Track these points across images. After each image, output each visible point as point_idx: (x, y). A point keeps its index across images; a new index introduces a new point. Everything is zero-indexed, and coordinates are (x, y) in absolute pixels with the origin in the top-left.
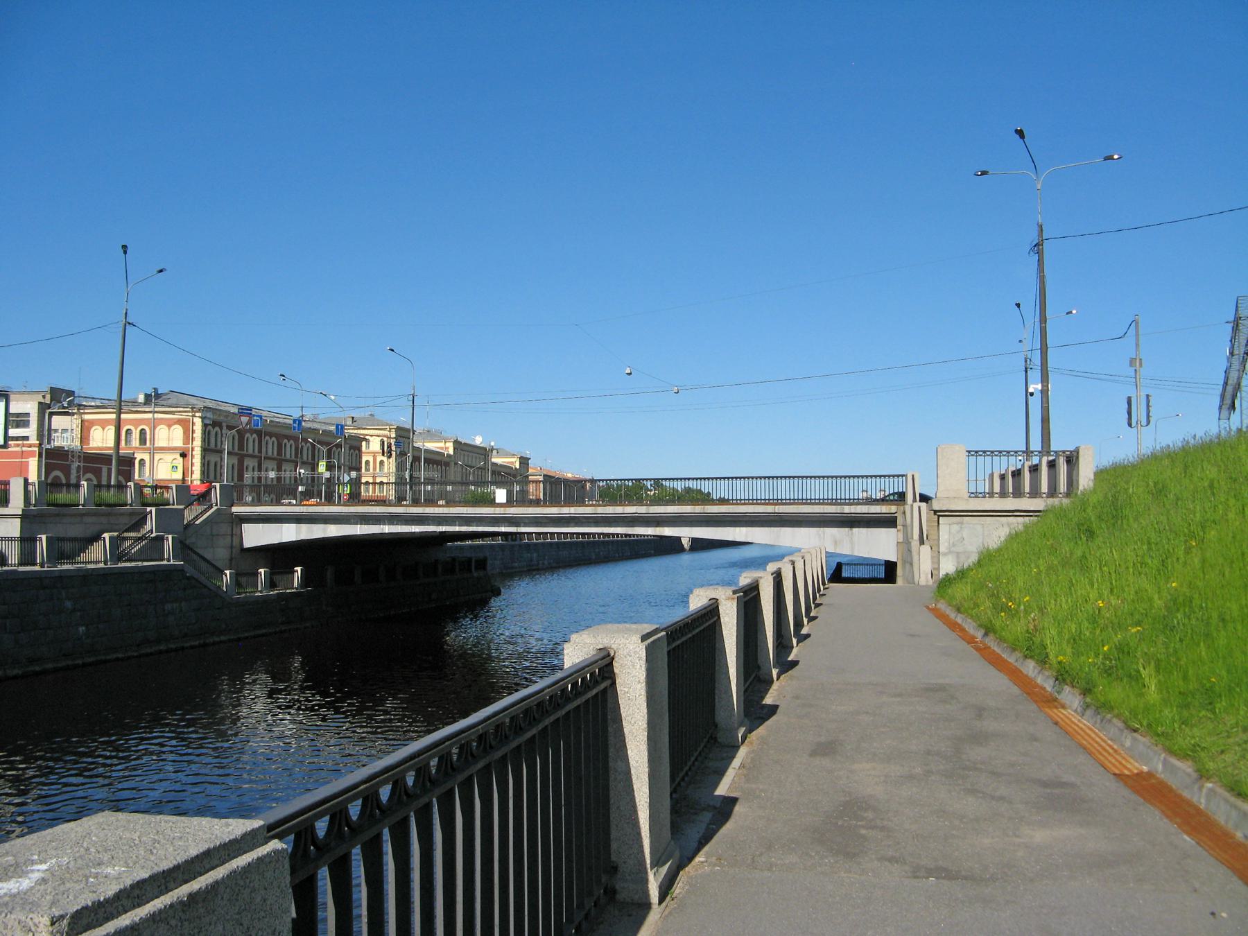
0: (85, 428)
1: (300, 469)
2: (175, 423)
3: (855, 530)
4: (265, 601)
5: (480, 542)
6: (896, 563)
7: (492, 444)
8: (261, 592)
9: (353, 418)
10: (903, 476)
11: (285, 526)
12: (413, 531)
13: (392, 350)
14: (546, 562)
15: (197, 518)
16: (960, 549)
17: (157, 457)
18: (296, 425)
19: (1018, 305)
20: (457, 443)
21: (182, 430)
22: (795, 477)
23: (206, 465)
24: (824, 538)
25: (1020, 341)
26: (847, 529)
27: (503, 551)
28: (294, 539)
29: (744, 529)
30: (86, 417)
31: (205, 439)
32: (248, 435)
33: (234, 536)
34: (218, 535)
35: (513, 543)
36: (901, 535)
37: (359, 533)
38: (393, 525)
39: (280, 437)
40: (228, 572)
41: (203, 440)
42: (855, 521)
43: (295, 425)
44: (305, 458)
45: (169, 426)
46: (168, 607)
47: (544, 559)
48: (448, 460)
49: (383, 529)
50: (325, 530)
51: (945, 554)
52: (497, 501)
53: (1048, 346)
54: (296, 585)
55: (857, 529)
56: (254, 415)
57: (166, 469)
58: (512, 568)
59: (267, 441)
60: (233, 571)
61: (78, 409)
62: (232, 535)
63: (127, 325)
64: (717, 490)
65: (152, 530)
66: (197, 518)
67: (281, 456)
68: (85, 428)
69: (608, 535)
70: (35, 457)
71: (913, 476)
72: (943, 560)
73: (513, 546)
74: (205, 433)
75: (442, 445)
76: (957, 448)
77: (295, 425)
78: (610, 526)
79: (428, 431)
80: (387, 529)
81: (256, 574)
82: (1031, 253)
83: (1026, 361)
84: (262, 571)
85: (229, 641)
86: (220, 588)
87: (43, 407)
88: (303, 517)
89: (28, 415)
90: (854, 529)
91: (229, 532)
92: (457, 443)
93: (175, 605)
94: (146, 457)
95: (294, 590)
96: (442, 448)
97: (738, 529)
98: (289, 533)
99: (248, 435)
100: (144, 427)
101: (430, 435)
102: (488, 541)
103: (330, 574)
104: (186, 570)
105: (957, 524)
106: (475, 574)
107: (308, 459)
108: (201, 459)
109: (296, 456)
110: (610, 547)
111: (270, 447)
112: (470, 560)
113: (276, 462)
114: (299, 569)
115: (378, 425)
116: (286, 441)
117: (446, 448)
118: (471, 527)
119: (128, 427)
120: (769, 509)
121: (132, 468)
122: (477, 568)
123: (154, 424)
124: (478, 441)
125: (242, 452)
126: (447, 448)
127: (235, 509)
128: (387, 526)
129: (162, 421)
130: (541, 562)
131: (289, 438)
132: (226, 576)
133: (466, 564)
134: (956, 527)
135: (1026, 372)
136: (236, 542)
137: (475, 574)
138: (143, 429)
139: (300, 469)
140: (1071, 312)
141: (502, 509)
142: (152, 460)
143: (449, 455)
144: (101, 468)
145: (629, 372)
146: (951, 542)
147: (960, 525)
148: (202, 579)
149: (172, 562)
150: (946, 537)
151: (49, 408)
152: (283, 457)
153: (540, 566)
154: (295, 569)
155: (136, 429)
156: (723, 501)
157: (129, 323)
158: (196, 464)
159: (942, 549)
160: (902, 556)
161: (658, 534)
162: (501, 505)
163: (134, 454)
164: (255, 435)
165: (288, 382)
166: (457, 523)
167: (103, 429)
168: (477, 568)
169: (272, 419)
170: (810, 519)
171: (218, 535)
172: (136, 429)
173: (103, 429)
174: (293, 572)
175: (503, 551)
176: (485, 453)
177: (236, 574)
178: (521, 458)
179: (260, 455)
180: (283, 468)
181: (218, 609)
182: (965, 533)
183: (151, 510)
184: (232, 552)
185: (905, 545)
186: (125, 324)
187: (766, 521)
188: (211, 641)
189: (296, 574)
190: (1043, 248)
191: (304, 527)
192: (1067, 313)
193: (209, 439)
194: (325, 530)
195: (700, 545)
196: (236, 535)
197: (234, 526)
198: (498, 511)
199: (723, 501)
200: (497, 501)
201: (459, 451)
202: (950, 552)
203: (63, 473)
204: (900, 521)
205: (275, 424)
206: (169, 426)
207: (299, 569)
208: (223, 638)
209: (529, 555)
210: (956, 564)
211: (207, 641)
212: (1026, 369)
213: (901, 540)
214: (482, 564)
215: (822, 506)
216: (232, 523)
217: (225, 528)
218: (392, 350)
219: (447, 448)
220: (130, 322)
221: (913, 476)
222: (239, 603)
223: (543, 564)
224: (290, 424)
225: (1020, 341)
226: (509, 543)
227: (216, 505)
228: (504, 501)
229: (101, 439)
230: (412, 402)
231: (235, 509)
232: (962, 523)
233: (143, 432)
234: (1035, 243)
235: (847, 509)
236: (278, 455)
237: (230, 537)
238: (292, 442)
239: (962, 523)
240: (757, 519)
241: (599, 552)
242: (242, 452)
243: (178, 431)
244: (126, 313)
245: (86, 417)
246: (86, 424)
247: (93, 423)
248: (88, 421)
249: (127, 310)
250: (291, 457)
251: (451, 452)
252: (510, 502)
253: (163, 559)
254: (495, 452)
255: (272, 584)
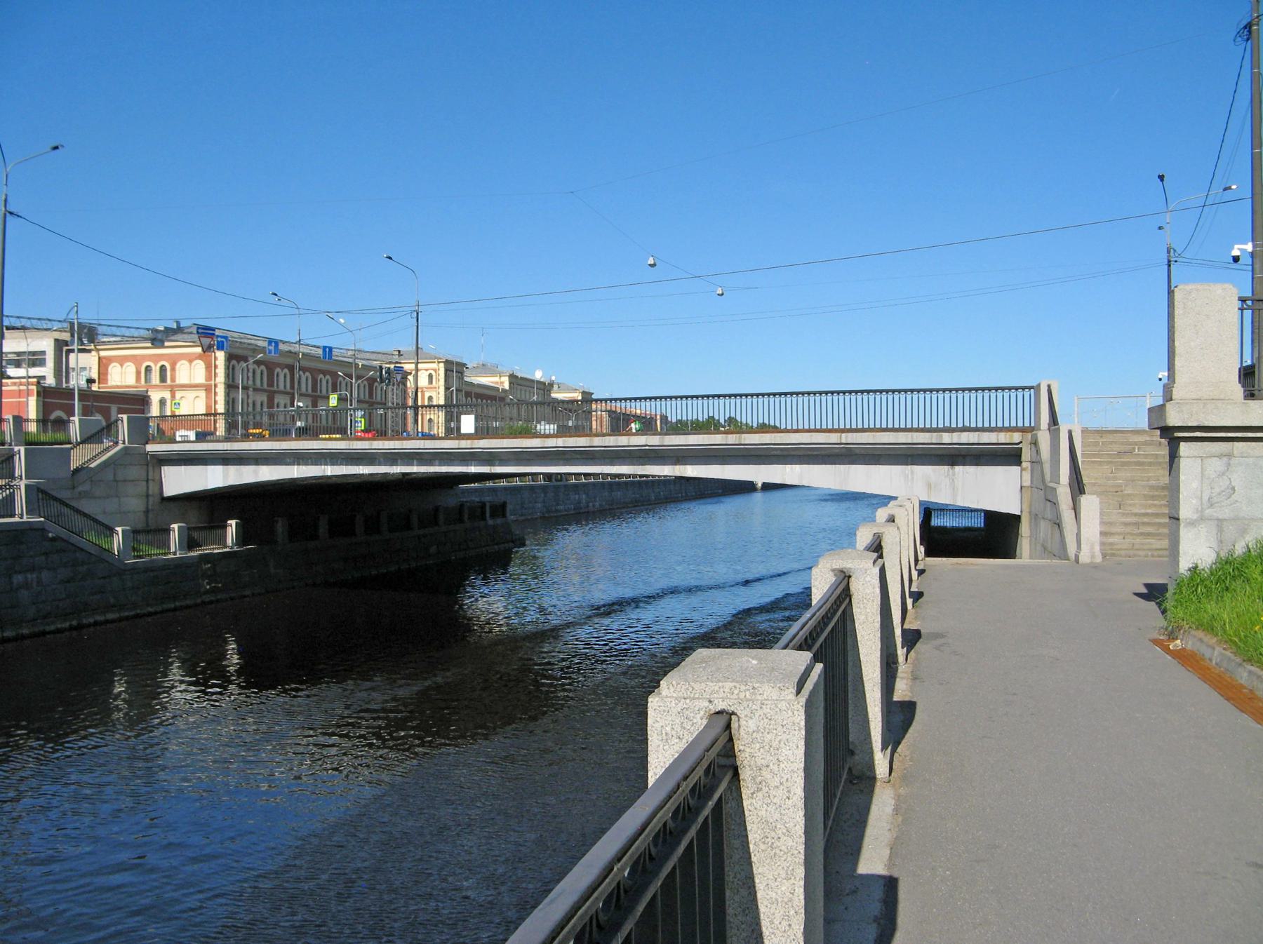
0: (103, 364)
1: (298, 401)
2: (196, 358)
3: (958, 468)
4: (179, 565)
5: (490, 484)
6: (1017, 518)
7: (553, 378)
8: (175, 553)
9: (399, 351)
10: (1030, 388)
11: (211, 468)
12: (361, 472)
13: (390, 258)
14: (597, 504)
15: (93, 459)
16: (1226, 513)
17: (178, 395)
18: (272, 348)
19: (1161, 178)
20: (513, 378)
21: (204, 366)
22: (871, 391)
23: (231, 402)
24: (913, 478)
25: (1160, 228)
26: (946, 467)
27: (545, 493)
28: (221, 485)
29: (797, 468)
30: (103, 353)
31: (228, 375)
32: (278, 370)
33: (150, 482)
34: (125, 481)
35: (559, 483)
36: (1027, 477)
37: (295, 476)
38: (337, 465)
39: (314, 372)
40: (119, 529)
41: (227, 376)
42: (959, 455)
43: (270, 348)
44: (303, 389)
45: (191, 361)
46: (17, 579)
47: (595, 501)
48: (503, 395)
49: (324, 471)
50: (256, 473)
51: (1192, 523)
52: (463, 431)
53: (1250, 200)
54: (229, 542)
55: (961, 467)
56: (218, 336)
57: (192, 404)
58: (557, 511)
59: (233, 366)
60: (128, 528)
61: (95, 346)
62: (147, 481)
63: (8, 214)
64: (747, 413)
65: (21, 476)
66: (93, 459)
67: (316, 392)
68: (103, 364)
69: (596, 475)
70: (33, 395)
71: (1049, 386)
72: (1186, 535)
73: (557, 487)
74: (228, 368)
75: (496, 379)
76: (1219, 291)
77: (270, 348)
78: (612, 464)
79: (483, 365)
80: (329, 470)
81: (167, 531)
82: (1239, 39)
83: (1169, 252)
84: (175, 526)
85: (120, 620)
86: (110, 551)
87: (59, 344)
88: (229, 456)
89: (43, 353)
90: (956, 467)
91: (144, 476)
92: (513, 378)
93: (31, 577)
94: (167, 395)
95: (228, 550)
96: (497, 383)
97: (788, 467)
98: (215, 478)
99: (278, 370)
100: (164, 363)
101: (484, 369)
102: (503, 483)
103: (281, 527)
104: (47, 528)
105: (1220, 456)
106: (490, 522)
107: (307, 390)
108: (225, 397)
109: (292, 387)
110: (672, 487)
111: (305, 379)
112: (483, 505)
113: (266, 394)
114: (233, 522)
115: (426, 359)
116: (321, 376)
117: (501, 383)
118: (432, 467)
119: (148, 363)
120: (833, 438)
121: (146, 407)
122: (492, 516)
123: (174, 360)
124: (538, 375)
125: (272, 389)
126: (502, 383)
127: (150, 448)
128: (329, 467)
129: (182, 357)
130: (591, 504)
131: (325, 373)
132: (118, 534)
133: (478, 512)
134: (1215, 465)
135: (1169, 266)
136: (153, 489)
137: (490, 522)
138: (163, 366)
139: (298, 401)
140: (1230, 188)
141: (469, 441)
142: (173, 397)
143: (504, 390)
144: (109, 407)
145: (652, 263)
146: (1206, 498)
147: (1225, 459)
148: (75, 539)
149: (25, 519)
150: (1195, 485)
151: (67, 345)
152: (275, 388)
153: (591, 509)
154: (229, 522)
155: (156, 365)
156: (764, 428)
157: (11, 213)
158: (219, 402)
159: (1185, 512)
160: (1030, 506)
161: (678, 474)
162: (468, 437)
163: (147, 391)
164: (286, 371)
165: (283, 302)
166: (415, 462)
167: (122, 366)
168: (492, 516)
169: (365, 362)
170: (823, 453)
171: (125, 481)
172: (156, 365)
173: (122, 366)
174: (225, 527)
175: (545, 493)
176: (546, 388)
177: (189, 529)
178: (583, 393)
179: (292, 391)
180: (276, 401)
181: (104, 578)
182: (1237, 479)
183: (19, 451)
184: (147, 502)
185: (1043, 491)
186: (5, 215)
187: (907, 456)
188: (92, 620)
189: (229, 529)
190: (1258, 30)
191: (232, 469)
192: (1225, 189)
193: (233, 374)
194: (256, 473)
195: (767, 487)
196: (153, 480)
197: (151, 468)
198: (465, 444)
199: (764, 428)
200: (463, 431)
201: (515, 386)
202: (1202, 519)
203: (63, 411)
204: (1026, 455)
205: (245, 346)
206: (191, 361)
207: (233, 522)
208: (110, 616)
209: (577, 496)
210: (1215, 545)
211: (85, 621)
212: (1169, 261)
213: (1027, 483)
214: (499, 510)
215: (910, 434)
216: (148, 465)
217: (135, 472)
218: (390, 258)
219: (502, 383)
220: (12, 210)
221: (1049, 386)
222: (134, 569)
223: (594, 506)
224: (265, 348)
225: (1160, 228)
226: (552, 484)
227: (124, 443)
228: (472, 431)
229: (122, 378)
230: (415, 320)
231: (150, 448)
232: (1230, 455)
233: (163, 369)
234: (1244, 23)
235: (947, 438)
236: (313, 391)
237: (144, 483)
238: (328, 377)
239: (1230, 455)
240: (810, 453)
241: (659, 493)
242: (272, 389)
243: (200, 366)
244: (6, 201)
245: (103, 353)
246: (104, 361)
247: (110, 360)
248: (105, 358)
249: (6, 195)
250: (307, 390)
251: (507, 386)
252: (481, 433)
253: (13, 516)
254: (555, 387)
255: (191, 544)
